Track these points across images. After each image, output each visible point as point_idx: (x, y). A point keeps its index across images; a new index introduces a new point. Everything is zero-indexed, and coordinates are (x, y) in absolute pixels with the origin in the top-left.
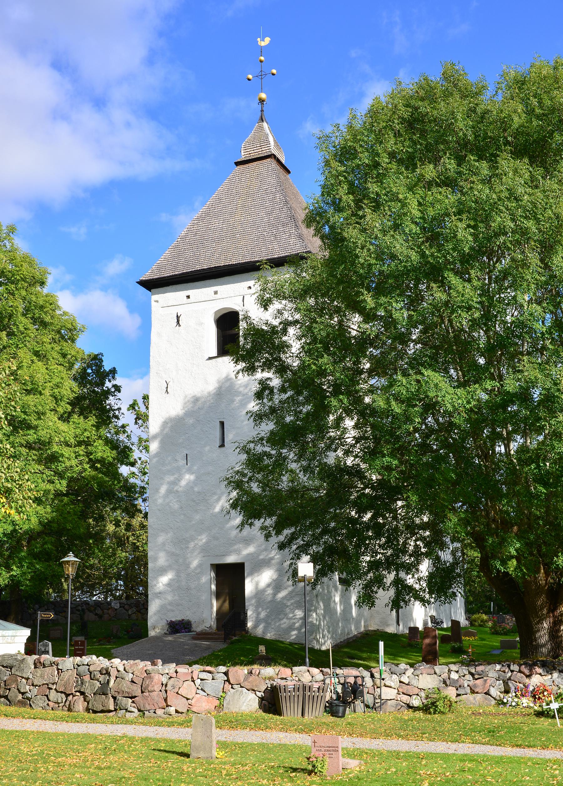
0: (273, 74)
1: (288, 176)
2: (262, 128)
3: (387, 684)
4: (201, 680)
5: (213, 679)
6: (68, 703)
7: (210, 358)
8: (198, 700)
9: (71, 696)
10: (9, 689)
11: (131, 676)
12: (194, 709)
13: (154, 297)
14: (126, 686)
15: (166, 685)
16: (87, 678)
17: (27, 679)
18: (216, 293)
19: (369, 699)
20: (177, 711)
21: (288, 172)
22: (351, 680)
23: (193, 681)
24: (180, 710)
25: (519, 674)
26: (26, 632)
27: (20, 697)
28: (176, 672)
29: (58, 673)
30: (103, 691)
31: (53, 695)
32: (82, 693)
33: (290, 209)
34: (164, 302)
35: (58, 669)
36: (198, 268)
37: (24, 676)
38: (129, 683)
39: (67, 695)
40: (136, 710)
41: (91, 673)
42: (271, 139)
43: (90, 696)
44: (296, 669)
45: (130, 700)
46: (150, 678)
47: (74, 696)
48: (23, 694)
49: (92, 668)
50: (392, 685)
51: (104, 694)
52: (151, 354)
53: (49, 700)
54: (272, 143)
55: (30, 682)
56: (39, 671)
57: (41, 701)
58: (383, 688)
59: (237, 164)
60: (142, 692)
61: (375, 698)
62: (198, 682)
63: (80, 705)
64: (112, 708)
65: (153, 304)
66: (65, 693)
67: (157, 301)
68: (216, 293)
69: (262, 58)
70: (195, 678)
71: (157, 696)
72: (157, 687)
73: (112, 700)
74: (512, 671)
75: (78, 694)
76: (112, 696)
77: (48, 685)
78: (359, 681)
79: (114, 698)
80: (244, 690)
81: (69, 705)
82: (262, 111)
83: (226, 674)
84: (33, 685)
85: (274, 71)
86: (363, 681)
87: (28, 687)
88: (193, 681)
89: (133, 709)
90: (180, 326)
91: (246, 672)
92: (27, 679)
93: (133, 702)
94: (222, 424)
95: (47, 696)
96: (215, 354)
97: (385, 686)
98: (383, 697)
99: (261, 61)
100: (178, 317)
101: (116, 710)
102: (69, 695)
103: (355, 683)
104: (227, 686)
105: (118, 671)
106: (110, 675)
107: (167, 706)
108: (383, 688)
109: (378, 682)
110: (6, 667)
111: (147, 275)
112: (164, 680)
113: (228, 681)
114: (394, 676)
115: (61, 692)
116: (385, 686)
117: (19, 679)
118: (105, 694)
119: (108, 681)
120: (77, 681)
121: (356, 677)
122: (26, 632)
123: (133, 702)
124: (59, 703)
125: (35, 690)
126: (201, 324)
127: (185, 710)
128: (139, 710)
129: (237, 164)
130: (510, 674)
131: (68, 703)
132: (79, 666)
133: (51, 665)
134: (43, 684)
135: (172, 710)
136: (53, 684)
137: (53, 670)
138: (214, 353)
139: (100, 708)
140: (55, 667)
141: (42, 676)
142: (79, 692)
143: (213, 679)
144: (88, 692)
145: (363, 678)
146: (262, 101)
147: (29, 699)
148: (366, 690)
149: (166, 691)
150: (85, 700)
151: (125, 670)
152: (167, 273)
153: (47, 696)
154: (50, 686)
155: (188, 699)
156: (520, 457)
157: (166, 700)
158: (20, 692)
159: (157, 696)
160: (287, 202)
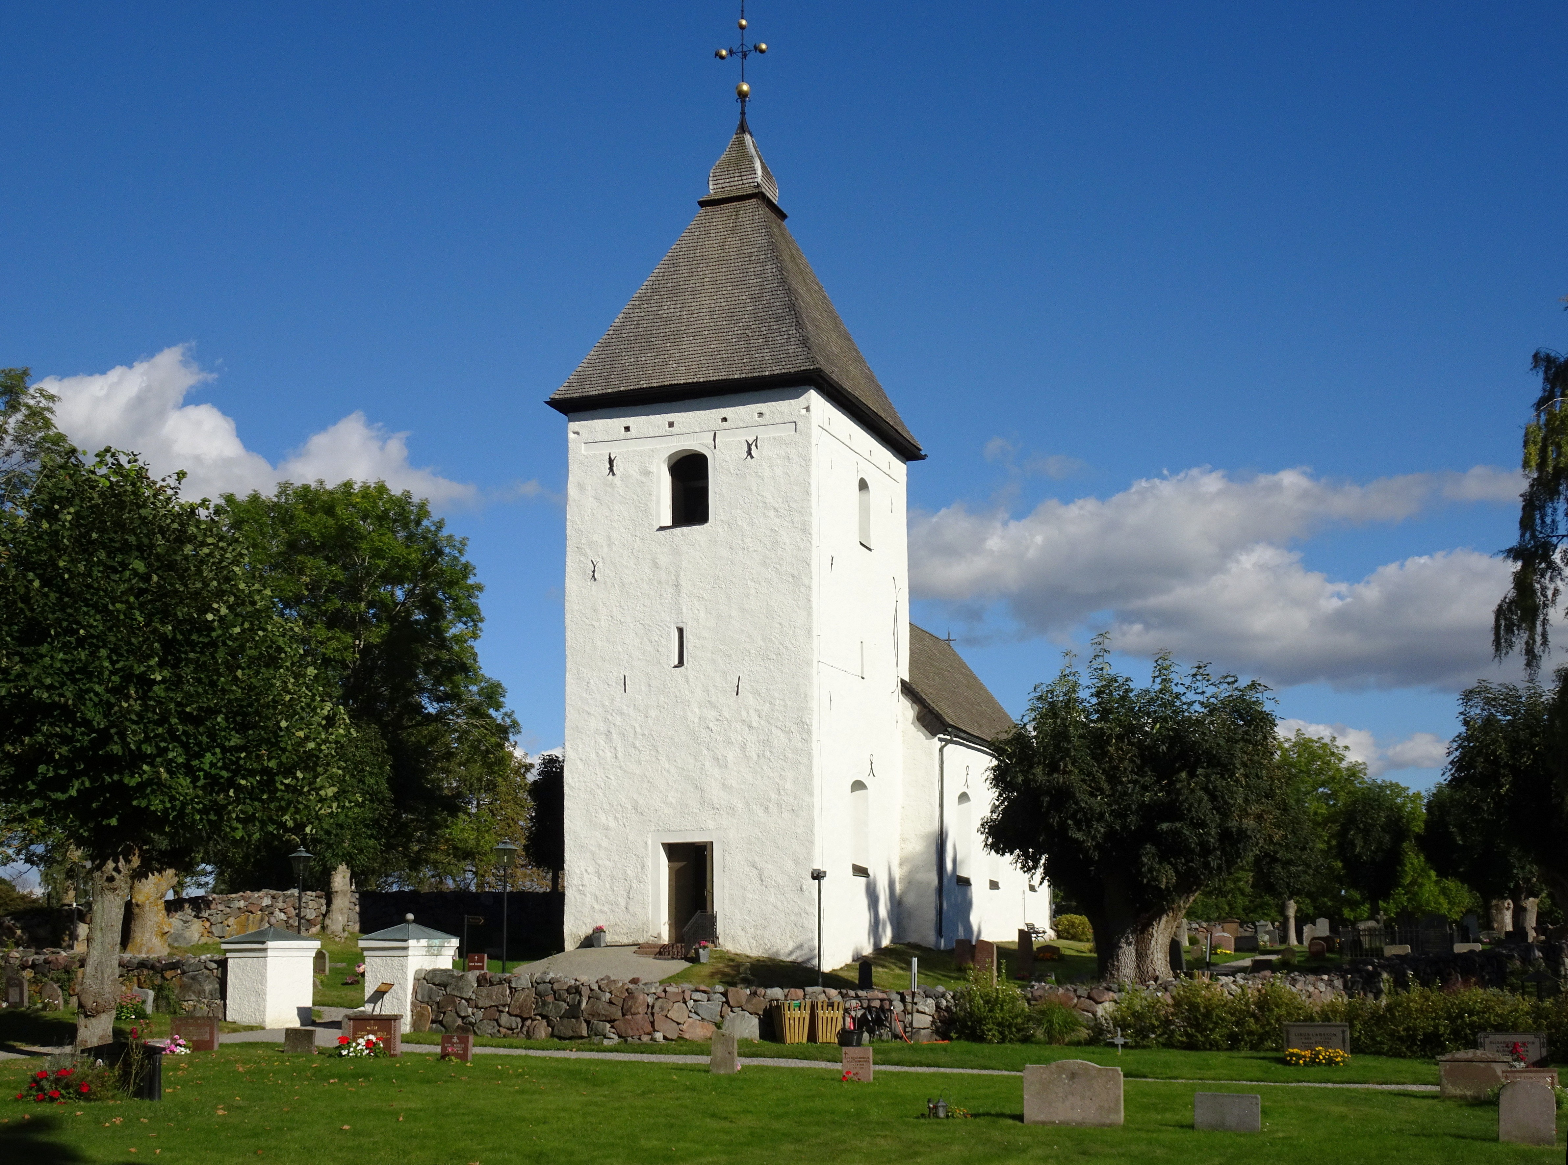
0: (762, 51)
1: (785, 223)
2: (741, 143)
3: (921, 1009)
4: (695, 1001)
5: (709, 1000)
6: (525, 1029)
7: (662, 528)
8: (691, 1025)
9: (530, 1021)
10: (444, 1013)
11: (608, 995)
12: (686, 1036)
13: (574, 426)
14: (602, 1007)
15: (653, 1007)
16: (550, 999)
17: (467, 1000)
18: (671, 425)
19: (899, 1028)
20: (665, 1038)
21: (783, 216)
22: (876, 1004)
23: (685, 1002)
24: (669, 1037)
25: (1088, 1001)
26: (455, 942)
27: (459, 1022)
28: (665, 991)
29: (511, 992)
30: (574, 1012)
31: (504, 1019)
32: (544, 1017)
33: (789, 291)
34: (589, 438)
35: (510, 988)
36: (644, 384)
37: (464, 996)
38: (606, 1005)
39: (524, 1020)
40: (615, 1037)
41: (555, 992)
42: (758, 165)
43: (556, 1020)
44: (809, 989)
45: (608, 1025)
46: (633, 998)
47: (533, 1020)
48: (463, 1018)
49: (556, 986)
50: (927, 1010)
51: (573, 1017)
52: (568, 517)
53: (499, 1025)
54: (759, 172)
55: (472, 1003)
56: (484, 990)
57: (489, 1028)
58: (916, 1015)
59: (702, 204)
60: (623, 1015)
61: (905, 1027)
62: (691, 1003)
63: (542, 1031)
64: (585, 1033)
65: (571, 436)
66: (521, 1017)
67: (578, 433)
68: (671, 425)
69: (744, 22)
70: (687, 998)
71: (641, 1018)
72: (642, 1010)
73: (584, 1025)
74: (1079, 997)
75: (539, 1017)
76: (585, 1021)
77: (497, 1006)
78: (886, 1005)
79: (588, 1022)
80: (747, 1014)
81: (528, 1032)
82: (743, 113)
83: (725, 994)
84: (477, 1007)
85: (764, 46)
86: (891, 1005)
87: (470, 1010)
88: (685, 1002)
89: (613, 1036)
90: (614, 474)
91: (748, 991)
92: (467, 1000)
93: (612, 1027)
94: (681, 631)
95: (497, 1021)
96: (670, 523)
97: (918, 1011)
98: (915, 1025)
99: (742, 28)
100: (611, 461)
101: (589, 1036)
102: (527, 1019)
103: (882, 1006)
104: (726, 1008)
105: (591, 990)
106: (581, 995)
107: (655, 1031)
108: (916, 1015)
109: (909, 1007)
110: (439, 985)
111: (561, 390)
112: (650, 1000)
113: (727, 1002)
114: (930, 1001)
115: (516, 1016)
116: (918, 1011)
117: (457, 1000)
118: (577, 1018)
119: (580, 1002)
120: (537, 1003)
121: (882, 1000)
122: (455, 942)
123: (612, 1027)
124: (512, 1029)
125: (480, 1014)
126: (647, 473)
127: (675, 1037)
128: (620, 1036)
129: (702, 204)
130: (1075, 1000)
131: (525, 1029)
132: (538, 984)
133: (500, 983)
134: (491, 1006)
135: (659, 1036)
136: (504, 1006)
137: (504, 990)
138: (667, 519)
139: (570, 1033)
140: (507, 985)
141: (489, 996)
142: (541, 1015)
143: (709, 1000)
144: (552, 1015)
145: (891, 1001)
146: (742, 96)
147: (472, 1024)
148: (894, 1016)
149: (653, 1014)
150: (548, 1025)
151: (600, 988)
152: (595, 391)
153: (497, 1021)
154: (501, 1008)
155: (678, 1024)
156: (1111, 713)
157: (652, 1023)
158: (459, 1016)
159: (641, 1018)
160: (783, 282)
